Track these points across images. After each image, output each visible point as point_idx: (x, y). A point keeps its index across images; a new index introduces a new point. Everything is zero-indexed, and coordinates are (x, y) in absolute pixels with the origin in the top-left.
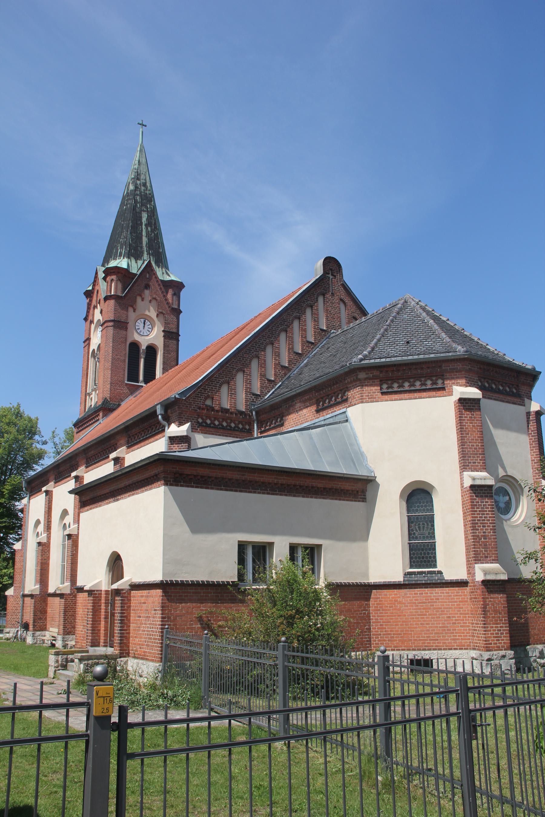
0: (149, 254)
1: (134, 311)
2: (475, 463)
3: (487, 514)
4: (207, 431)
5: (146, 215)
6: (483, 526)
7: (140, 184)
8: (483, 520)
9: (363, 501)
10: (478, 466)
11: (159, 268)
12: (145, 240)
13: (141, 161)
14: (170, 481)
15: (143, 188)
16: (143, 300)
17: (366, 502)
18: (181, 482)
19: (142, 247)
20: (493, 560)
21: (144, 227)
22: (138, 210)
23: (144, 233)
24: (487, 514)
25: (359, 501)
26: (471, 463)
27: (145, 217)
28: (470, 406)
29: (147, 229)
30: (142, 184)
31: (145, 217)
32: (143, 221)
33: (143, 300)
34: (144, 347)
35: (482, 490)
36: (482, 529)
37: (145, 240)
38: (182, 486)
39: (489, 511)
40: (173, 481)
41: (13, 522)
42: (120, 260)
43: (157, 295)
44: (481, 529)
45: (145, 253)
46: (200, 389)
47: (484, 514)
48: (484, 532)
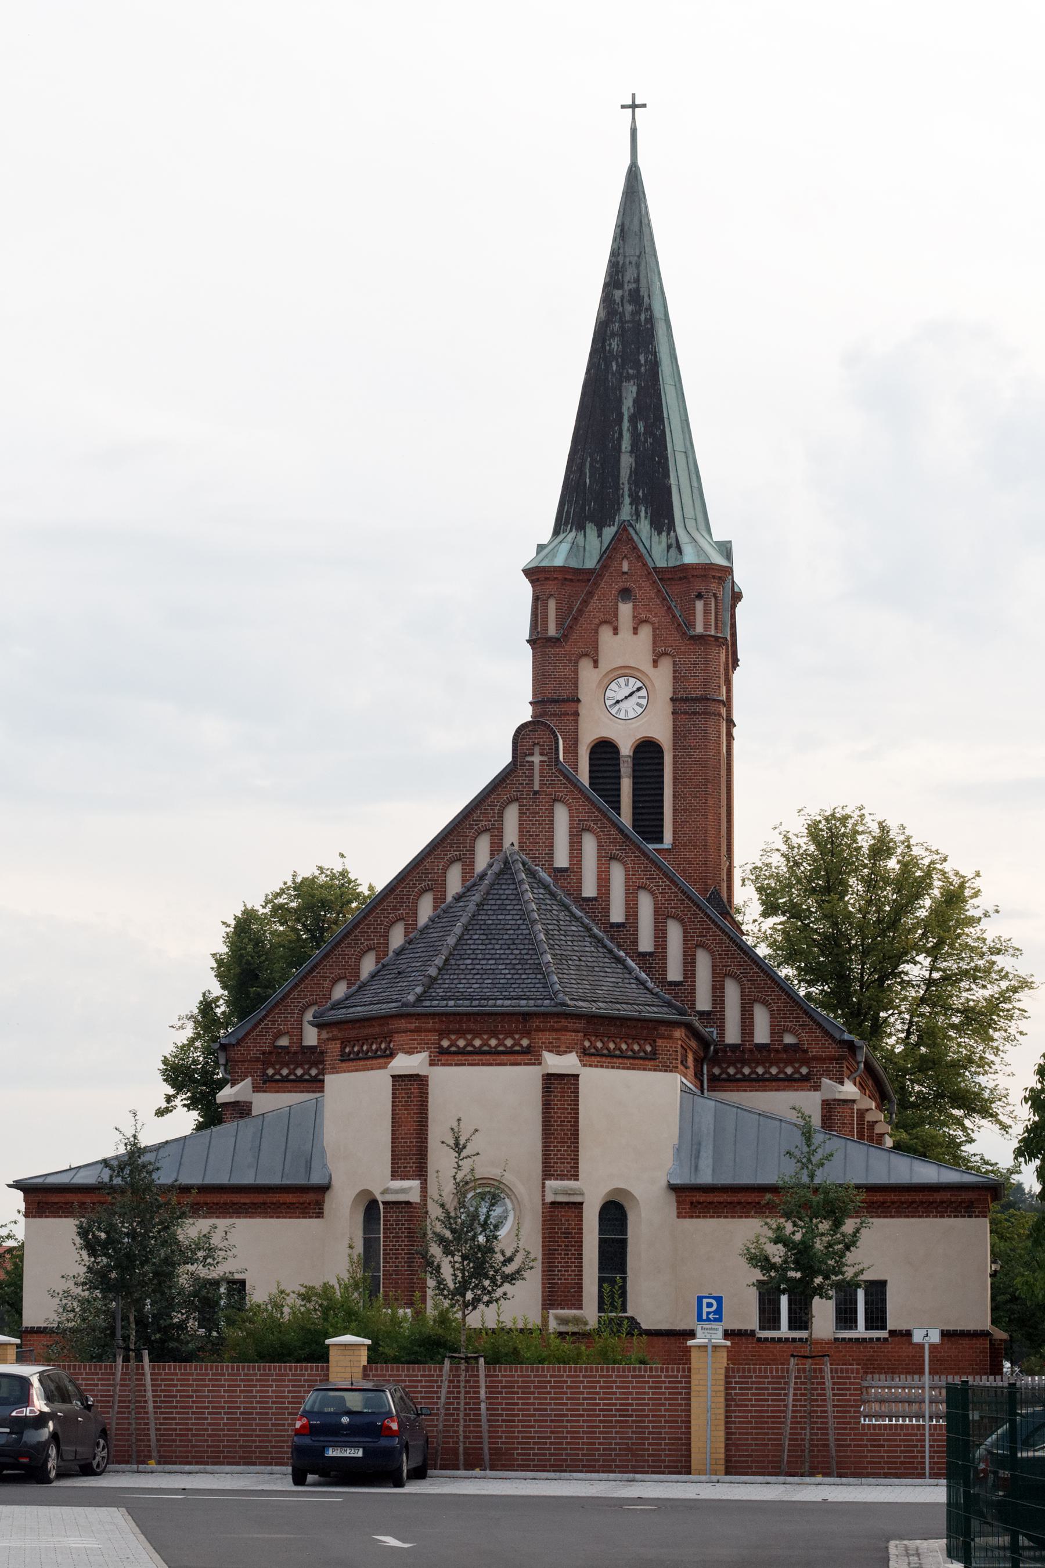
0: (635, 501)
1: (596, 666)
2: (406, 1167)
3: (402, 1241)
4: (279, 1087)
5: (634, 389)
6: (396, 1258)
7: (622, 298)
8: (396, 1250)
9: (319, 1217)
10: (409, 1171)
11: (659, 533)
12: (626, 461)
13: (627, 223)
14: (32, 1213)
15: (629, 308)
16: (616, 631)
17: (323, 1217)
18: (45, 1212)
19: (617, 486)
20: (405, 1304)
21: (626, 424)
22: (612, 380)
23: (626, 444)
24: (402, 1241)
25: (311, 1217)
26: (400, 1167)
27: (630, 393)
28: (407, 1085)
29: (635, 428)
30: (627, 298)
31: (630, 393)
32: (625, 410)
33: (616, 631)
34: (626, 749)
35: (398, 1208)
36: (395, 1262)
37: (626, 461)
38: (46, 1217)
39: (405, 1237)
40: (36, 1212)
41: (967, 1050)
42: (565, 534)
43: (649, 611)
44: (393, 1262)
45: (627, 500)
46: (266, 1022)
47: (398, 1241)
48: (397, 1266)
